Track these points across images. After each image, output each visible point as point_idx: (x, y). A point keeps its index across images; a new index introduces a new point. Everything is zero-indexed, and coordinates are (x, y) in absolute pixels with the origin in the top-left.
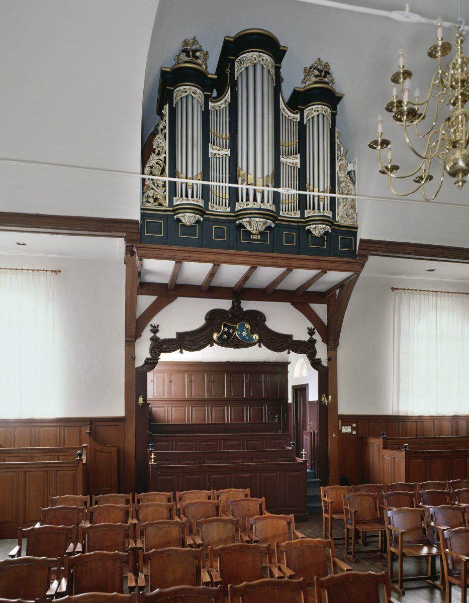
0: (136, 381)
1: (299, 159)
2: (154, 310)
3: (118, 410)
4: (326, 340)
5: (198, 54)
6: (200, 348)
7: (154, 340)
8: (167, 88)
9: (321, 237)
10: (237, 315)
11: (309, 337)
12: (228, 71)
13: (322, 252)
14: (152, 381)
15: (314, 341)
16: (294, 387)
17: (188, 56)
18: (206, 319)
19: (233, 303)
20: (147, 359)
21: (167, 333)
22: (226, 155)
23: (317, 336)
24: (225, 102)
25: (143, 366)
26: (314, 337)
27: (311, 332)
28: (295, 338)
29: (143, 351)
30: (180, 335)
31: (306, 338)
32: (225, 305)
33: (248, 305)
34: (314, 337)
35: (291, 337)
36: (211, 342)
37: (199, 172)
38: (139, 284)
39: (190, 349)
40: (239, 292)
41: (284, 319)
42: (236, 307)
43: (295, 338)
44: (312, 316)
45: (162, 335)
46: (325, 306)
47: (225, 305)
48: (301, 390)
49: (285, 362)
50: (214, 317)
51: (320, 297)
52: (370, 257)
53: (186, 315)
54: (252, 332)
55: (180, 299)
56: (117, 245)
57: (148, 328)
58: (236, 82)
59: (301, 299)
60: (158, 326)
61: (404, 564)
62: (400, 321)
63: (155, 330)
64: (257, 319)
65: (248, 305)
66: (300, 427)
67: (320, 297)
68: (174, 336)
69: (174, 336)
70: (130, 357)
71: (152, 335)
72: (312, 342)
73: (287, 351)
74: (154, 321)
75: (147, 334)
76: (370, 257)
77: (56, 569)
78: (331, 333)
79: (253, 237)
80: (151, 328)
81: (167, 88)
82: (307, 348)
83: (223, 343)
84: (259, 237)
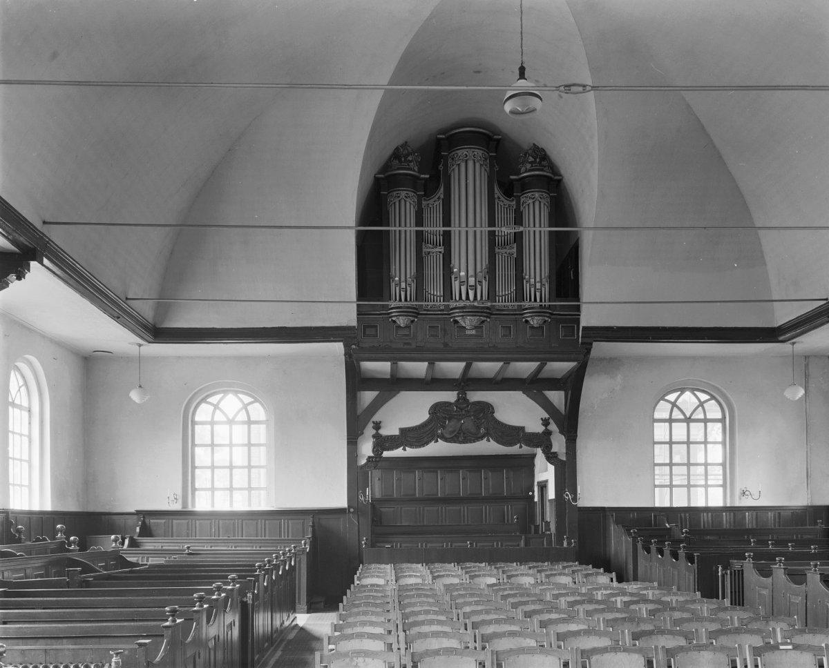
1: (515, 248)
2: (376, 406)
6: (423, 445)
7: (377, 437)
11: (544, 428)
12: (441, 167)
14: (379, 479)
16: (538, 483)
17: (400, 161)
18: (429, 414)
19: (458, 394)
20: (369, 457)
22: (440, 252)
23: (553, 427)
24: (439, 198)
25: (366, 464)
26: (550, 427)
27: (546, 423)
29: (366, 448)
30: (402, 430)
31: (539, 428)
32: (450, 396)
33: (475, 396)
34: (550, 427)
35: (523, 428)
37: (412, 274)
38: (356, 381)
39: (411, 446)
40: (465, 383)
41: (518, 410)
42: (462, 399)
44: (547, 405)
45: (384, 432)
46: (562, 393)
47: (450, 396)
48: (543, 486)
49: (532, 455)
50: (436, 409)
51: (554, 383)
52: (595, 344)
53: (411, 410)
55: (521, 392)
56: (338, 347)
57: (371, 425)
58: (450, 176)
59: (534, 386)
60: (380, 422)
63: (377, 426)
64: (486, 409)
65: (475, 396)
66: (194, 558)
67: (554, 383)
68: (397, 433)
69: (397, 433)
71: (374, 432)
72: (548, 433)
73: (518, 445)
74: (376, 418)
75: (369, 431)
76: (595, 344)
77: (512, 177)
78: (569, 422)
79: (468, 332)
80: (373, 425)
82: (542, 440)
84: (474, 332)
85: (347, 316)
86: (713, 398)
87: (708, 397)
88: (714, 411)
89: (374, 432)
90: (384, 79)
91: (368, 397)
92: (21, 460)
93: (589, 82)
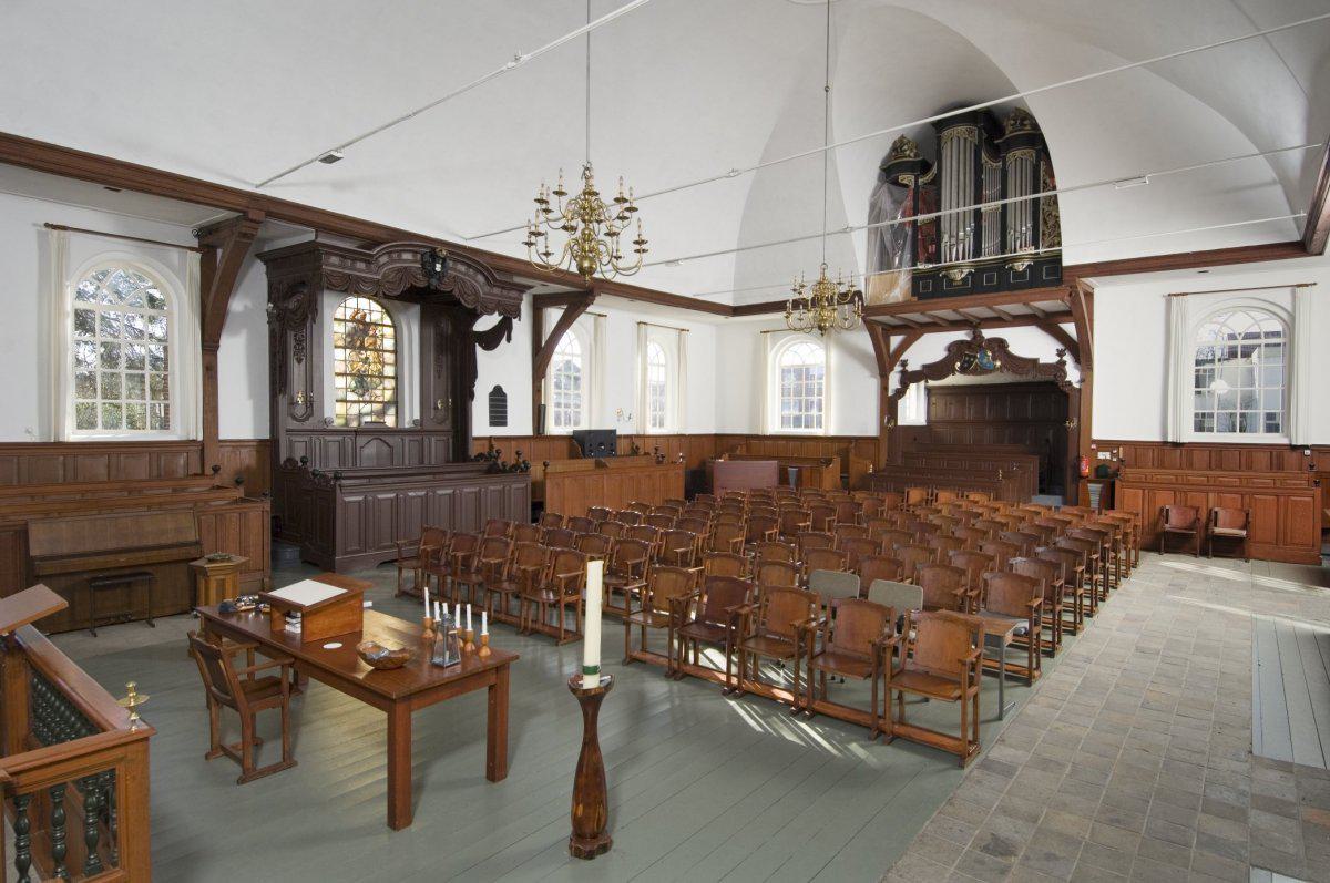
0: (889, 406)
3: (872, 430)
4: (1077, 361)
5: (1026, 122)
7: (904, 373)
8: (595, 571)
9: (1024, 271)
10: (977, 344)
13: (1031, 285)
15: (1065, 363)
21: (914, 366)
23: (1068, 358)
26: (1065, 358)
27: (1060, 354)
28: (1041, 362)
29: (894, 381)
30: (925, 366)
32: (962, 335)
33: (988, 333)
34: (1065, 358)
35: (1035, 361)
36: (953, 371)
43: (1041, 362)
44: (1061, 336)
45: (910, 368)
47: (962, 335)
50: (956, 349)
54: (994, 359)
55: (1034, 327)
61: (824, 360)
62: (59, 391)
63: (904, 364)
65: (988, 333)
70: (884, 387)
74: (903, 358)
75: (898, 368)
81: (595, 571)
83: (963, 370)
85: (553, 428)
86: (394, 326)
87: (390, 323)
88: (387, 321)
89: (900, 368)
90: (866, 224)
91: (895, 341)
92: (658, 365)
93: (549, 470)
